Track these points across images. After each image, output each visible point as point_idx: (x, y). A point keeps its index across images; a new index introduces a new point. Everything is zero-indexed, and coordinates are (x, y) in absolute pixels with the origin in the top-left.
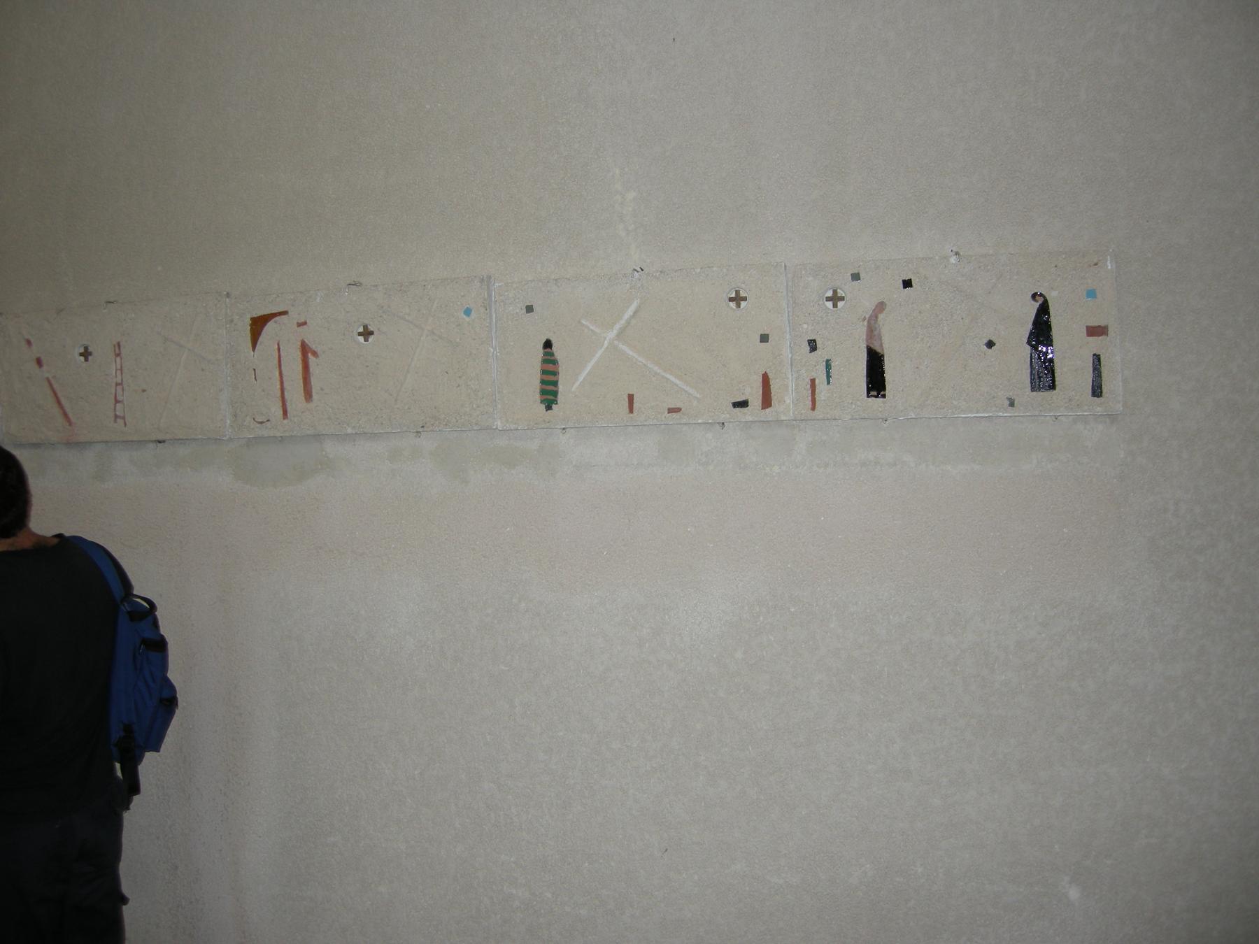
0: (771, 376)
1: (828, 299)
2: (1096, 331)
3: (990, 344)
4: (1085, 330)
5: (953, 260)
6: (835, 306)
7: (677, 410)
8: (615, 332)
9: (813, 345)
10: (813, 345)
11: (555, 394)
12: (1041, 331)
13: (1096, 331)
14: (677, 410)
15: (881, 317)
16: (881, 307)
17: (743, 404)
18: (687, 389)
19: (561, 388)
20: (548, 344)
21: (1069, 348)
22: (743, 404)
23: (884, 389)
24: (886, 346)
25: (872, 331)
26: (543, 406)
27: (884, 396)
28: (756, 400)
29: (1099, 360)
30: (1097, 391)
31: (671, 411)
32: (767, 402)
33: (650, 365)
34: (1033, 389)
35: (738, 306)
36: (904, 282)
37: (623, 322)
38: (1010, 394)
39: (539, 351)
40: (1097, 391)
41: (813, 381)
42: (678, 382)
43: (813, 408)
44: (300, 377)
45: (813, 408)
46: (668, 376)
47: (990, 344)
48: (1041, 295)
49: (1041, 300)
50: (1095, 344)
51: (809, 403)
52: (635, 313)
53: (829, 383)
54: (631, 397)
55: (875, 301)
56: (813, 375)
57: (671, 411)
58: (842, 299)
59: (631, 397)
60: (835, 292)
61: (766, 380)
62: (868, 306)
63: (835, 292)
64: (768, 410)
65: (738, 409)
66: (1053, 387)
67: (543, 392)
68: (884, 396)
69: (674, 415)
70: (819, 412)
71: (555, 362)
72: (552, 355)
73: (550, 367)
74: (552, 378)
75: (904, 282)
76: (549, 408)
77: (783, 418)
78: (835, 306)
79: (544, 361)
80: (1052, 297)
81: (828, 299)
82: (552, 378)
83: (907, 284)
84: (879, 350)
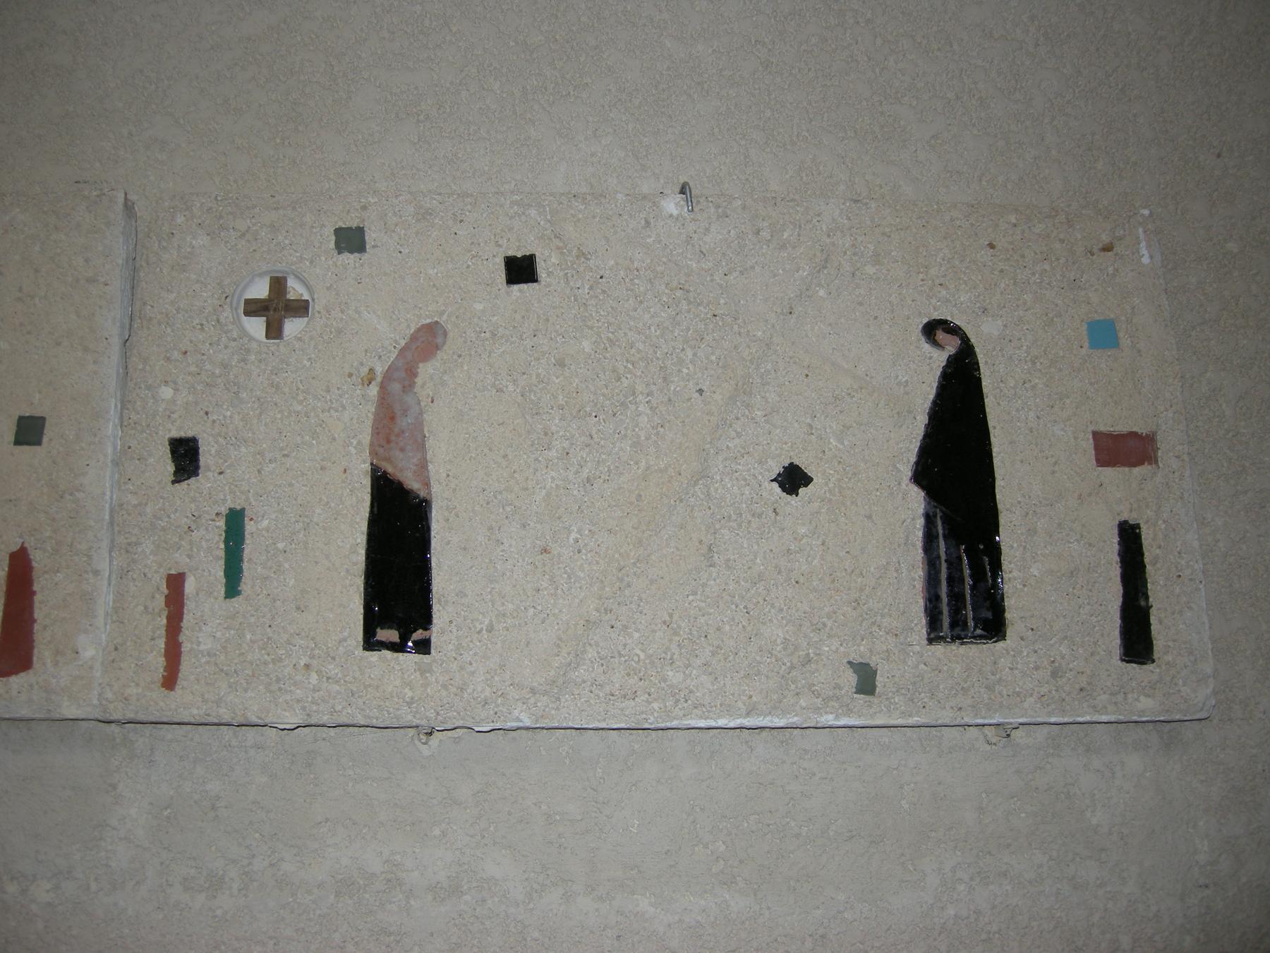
0: (38, 559)
1: (253, 308)
2: (1122, 450)
3: (793, 479)
4: (1088, 444)
5: (672, 205)
6: (274, 331)
9: (186, 456)
10: (186, 456)
12: (955, 461)
13: (1122, 450)
15: (426, 371)
16: (428, 340)
23: (426, 620)
24: (436, 470)
25: (392, 421)
27: (424, 647)
29: (1137, 537)
30: (1137, 641)
34: (931, 641)
36: (807, 480)
38: (860, 652)
40: (1137, 641)
41: (176, 583)
43: (170, 681)
45: (170, 681)
47: (793, 479)
48: (954, 330)
49: (951, 346)
50: (1122, 491)
51: (158, 662)
53: (232, 589)
55: (411, 322)
56: (179, 561)
58: (301, 308)
60: (278, 284)
62: (380, 333)
63: (278, 284)
66: (994, 627)
68: (424, 647)
70: (188, 700)
75: (807, 480)
77: (70, 711)
78: (274, 331)
80: (983, 334)
81: (253, 308)
83: (521, 270)
84: (413, 484)
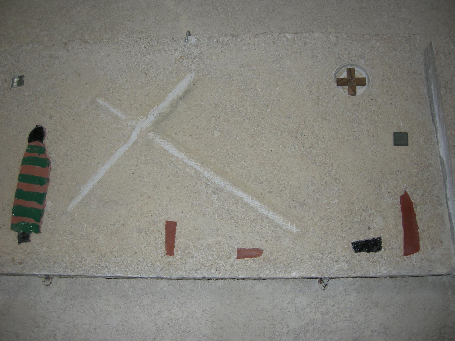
0: (415, 199)
7: (253, 253)
8: (151, 118)
11: (38, 215)
14: (253, 253)
17: (371, 246)
18: (272, 215)
19: (49, 203)
20: (38, 134)
21: (248, 267)
22: (371, 246)
26: (14, 235)
28: (393, 239)
31: (243, 254)
32: (411, 243)
33: (208, 174)
35: (353, 92)
37: (166, 104)
39: (22, 145)
42: (255, 203)
44: (163, 239)
46: (239, 193)
52: (187, 92)
54: (171, 228)
57: (243, 254)
59: (171, 228)
61: (407, 207)
64: (415, 257)
65: (363, 255)
67: (18, 211)
69: (249, 262)
71: (45, 163)
72: (43, 150)
73: (36, 170)
74: (36, 188)
76: (24, 238)
79: (26, 161)
82: (36, 188)
